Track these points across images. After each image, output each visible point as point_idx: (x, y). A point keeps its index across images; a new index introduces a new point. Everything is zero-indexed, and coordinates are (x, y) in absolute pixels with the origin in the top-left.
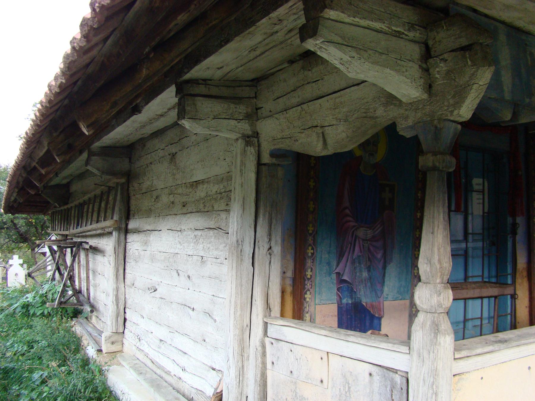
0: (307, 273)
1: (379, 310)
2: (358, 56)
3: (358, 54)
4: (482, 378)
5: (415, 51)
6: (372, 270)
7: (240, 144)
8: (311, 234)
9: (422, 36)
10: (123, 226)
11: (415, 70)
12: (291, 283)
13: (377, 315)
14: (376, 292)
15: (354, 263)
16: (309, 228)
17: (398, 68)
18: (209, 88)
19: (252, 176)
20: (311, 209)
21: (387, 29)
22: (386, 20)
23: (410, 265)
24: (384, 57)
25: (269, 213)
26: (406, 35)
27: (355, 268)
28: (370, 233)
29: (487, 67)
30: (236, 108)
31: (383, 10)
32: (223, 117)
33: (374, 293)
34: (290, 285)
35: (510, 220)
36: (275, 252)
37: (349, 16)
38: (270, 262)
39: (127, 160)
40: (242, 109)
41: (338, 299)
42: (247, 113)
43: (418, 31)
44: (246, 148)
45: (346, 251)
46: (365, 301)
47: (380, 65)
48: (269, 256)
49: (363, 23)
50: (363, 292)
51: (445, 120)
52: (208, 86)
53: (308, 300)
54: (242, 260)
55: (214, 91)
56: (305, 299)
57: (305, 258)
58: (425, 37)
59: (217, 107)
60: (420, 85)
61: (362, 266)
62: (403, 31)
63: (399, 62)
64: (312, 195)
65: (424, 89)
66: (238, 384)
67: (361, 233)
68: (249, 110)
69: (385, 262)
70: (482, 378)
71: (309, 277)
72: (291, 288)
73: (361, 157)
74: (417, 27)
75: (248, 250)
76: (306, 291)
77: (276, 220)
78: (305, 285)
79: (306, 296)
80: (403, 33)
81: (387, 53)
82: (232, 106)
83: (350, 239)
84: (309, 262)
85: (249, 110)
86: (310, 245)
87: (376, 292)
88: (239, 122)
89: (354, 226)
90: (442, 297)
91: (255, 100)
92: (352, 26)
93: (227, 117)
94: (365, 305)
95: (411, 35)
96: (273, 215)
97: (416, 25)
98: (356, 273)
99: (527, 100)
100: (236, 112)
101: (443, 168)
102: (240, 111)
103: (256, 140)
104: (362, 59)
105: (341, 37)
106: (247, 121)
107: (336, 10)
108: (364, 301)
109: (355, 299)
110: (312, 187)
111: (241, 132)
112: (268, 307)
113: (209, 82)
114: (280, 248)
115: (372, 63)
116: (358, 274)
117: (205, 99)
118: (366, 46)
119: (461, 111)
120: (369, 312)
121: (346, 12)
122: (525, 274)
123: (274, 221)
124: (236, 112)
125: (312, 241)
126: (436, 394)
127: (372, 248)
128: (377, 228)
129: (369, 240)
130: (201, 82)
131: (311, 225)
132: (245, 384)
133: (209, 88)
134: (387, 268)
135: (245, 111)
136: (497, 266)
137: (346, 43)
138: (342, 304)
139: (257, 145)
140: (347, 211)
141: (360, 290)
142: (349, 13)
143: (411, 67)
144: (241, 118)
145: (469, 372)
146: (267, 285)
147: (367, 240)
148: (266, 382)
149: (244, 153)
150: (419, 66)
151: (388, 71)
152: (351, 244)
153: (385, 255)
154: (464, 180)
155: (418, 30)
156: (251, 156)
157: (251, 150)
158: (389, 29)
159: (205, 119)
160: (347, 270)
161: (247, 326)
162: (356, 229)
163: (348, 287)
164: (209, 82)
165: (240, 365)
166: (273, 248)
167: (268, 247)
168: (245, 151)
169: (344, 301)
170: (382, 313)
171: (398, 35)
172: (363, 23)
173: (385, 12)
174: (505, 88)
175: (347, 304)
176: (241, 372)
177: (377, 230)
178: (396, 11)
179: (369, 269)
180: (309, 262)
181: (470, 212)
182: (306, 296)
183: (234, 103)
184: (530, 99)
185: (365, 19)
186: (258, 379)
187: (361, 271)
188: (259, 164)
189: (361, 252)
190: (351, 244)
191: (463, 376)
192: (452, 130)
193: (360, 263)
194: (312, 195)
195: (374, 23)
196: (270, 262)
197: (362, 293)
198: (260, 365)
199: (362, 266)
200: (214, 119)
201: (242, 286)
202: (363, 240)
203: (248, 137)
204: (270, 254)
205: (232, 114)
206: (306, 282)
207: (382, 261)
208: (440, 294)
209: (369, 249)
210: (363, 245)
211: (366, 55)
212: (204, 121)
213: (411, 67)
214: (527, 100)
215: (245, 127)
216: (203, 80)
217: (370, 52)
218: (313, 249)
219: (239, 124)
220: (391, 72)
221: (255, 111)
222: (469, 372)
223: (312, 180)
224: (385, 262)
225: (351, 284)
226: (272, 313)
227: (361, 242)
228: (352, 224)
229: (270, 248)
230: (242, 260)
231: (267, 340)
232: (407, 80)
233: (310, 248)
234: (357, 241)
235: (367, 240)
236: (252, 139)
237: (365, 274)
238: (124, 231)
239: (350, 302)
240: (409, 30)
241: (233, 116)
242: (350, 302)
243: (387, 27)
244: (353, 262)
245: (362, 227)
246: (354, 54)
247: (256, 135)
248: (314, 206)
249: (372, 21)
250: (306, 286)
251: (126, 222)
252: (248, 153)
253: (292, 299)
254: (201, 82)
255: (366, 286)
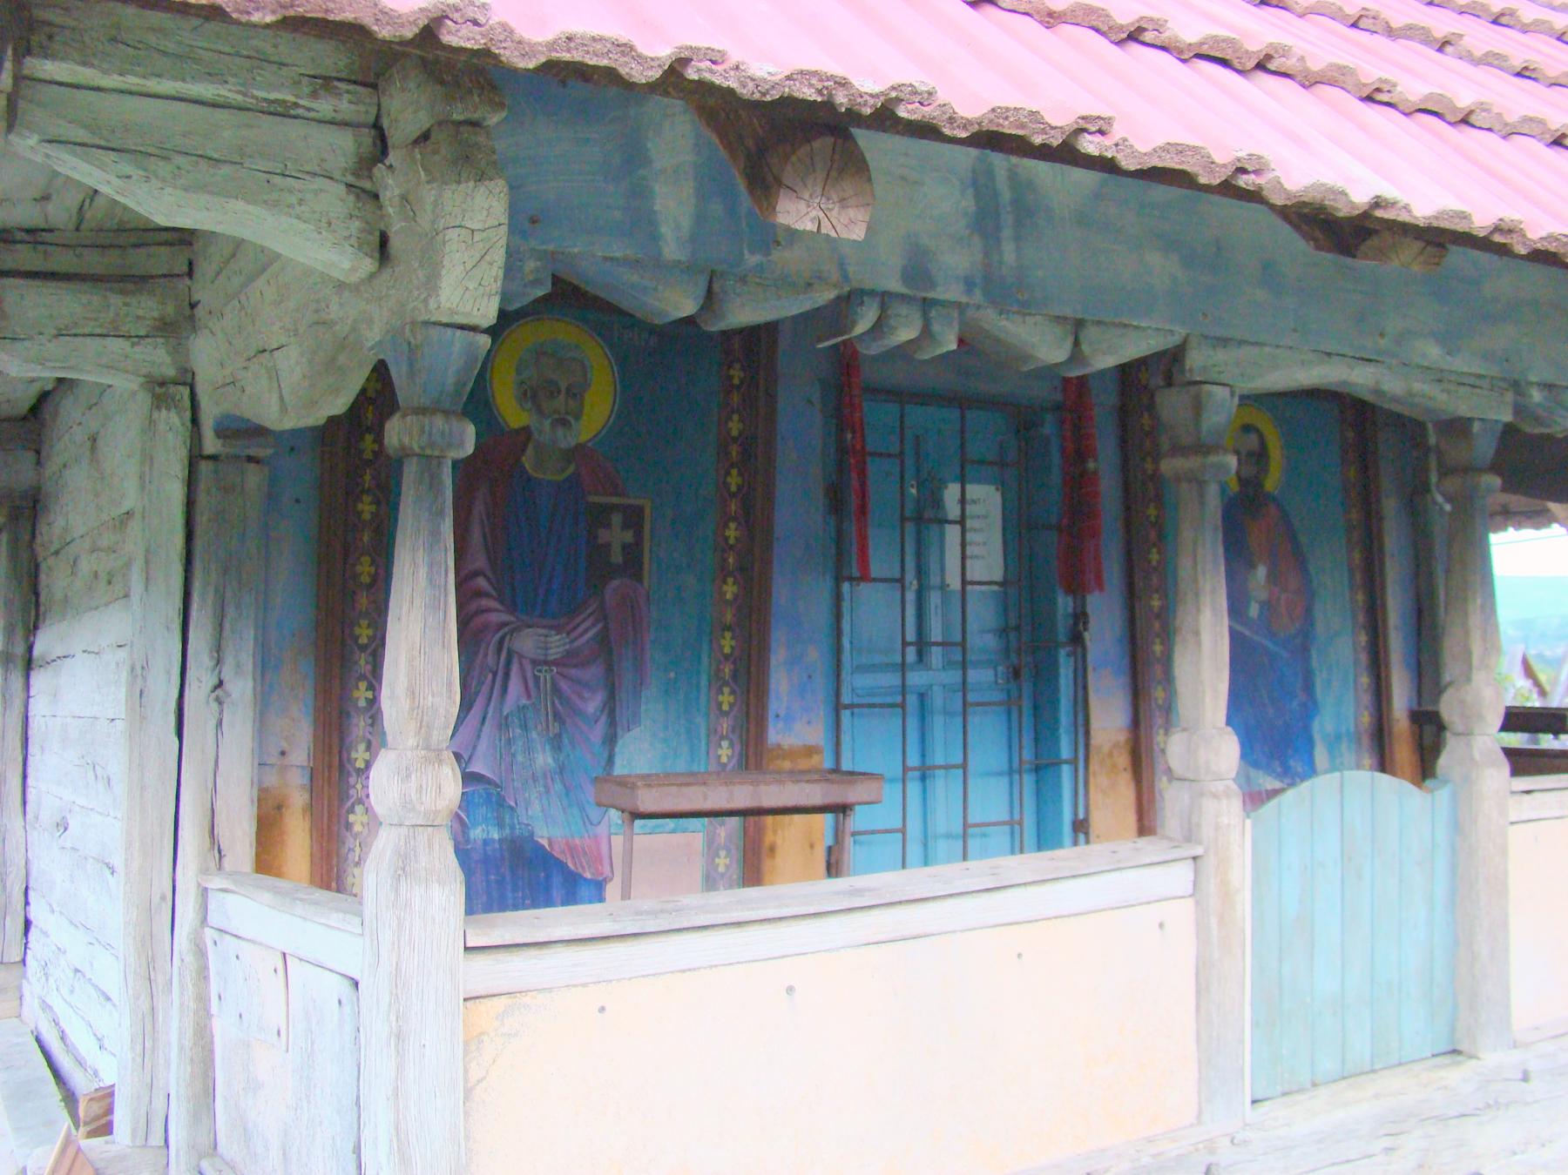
0: (354, 755)
1: (598, 859)
2: (142, 173)
3: (139, 168)
4: (602, 1009)
5: (343, 147)
6: (567, 749)
7: (144, 399)
8: (363, 648)
9: (362, 108)
10: (20, 649)
11: (333, 199)
12: (306, 780)
13: (588, 875)
14: (582, 810)
15: (507, 726)
16: (357, 631)
17: (275, 195)
18: (45, 252)
19: (175, 492)
20: (366, 579)
21: (240, 98)
22: (235, 75)
23: (703, 732)
24: (226, 170)
25: (217, 591)
26: (309, 109)
27: (509, 742)
28: (557, 644)
29: (471, 184)
30: (127, 304)
31: (228, 49)
32: (87, 331)
33: (576, 811)
34: (303, 787)
35: (1064, 604)
36: (235, 695)
37: (106, 72)
38: (220, 723)
39: (30, 457)
40: (147, 307)
41: (457, 826)
42: (162, 319)
43: (346, 97)
44: (156, 415)
45: (477, 694)
46: (546, 834)
47: (212, 193)
48: (215, 706)
49: (167, 86)
50: (538, 807)
51: (426, 323)
52: (40, 247)
53: (357, 828)
54: (143, 718)
55: (63, 261)
56: (349, 826)
57: (348, 714)
58: (374, 111)
59: (68, 303)
60: (346, 238)
61: (534, 735)
62: (292, 99)
63: (278, 180)
64: (366, 539)
65: (360, 248)
66: (140, 1060)
67: (527, 643)
68: (170, 310)
69: (612, 723)
70: (602, 1009)
71: (360, 764)
72: (307, 796)
73: (526, 431)
74: (343, 86)
75: (164, 690)
76: (353, 806)
77: (238, 607)
78: (349, 787)
79: (352, 818)
80: (296, 105)
81: (238, 159)
82: (116, 300)
83: (491, 660)
84: (362, 724)
85: (170, 310)
86: (363, 677)
87: (582, 810)
88: (133, 345)
89: (505, 624)
90: (413, 783)
91: (188, 282)
92: (128, 97)
93: (98, 331)
94: (545, 843)
95: (325, 107)
96: (229, 594)
97: (339, 80)
98: (514, 755)
99: (752, 260)
100: (127, 315)
101: (422, 448)
102: (140, 312)
103: (186, 391)
104: (154, 180)
105: (86, 127)
106: (160, 340)
107: (62, 59)
108: (543, 835)
109: (512, 828)
110: (367, 516)
111: (144, 371)
112: (215, 846)
113: (47, 237)
114: (250, 684)
115: (186, 190)
116: (520, 758)
117: (30, 282)
118: (168, 146)
119: (443, 298)
120: (562, 865)
121: (96, 62)
122: (1123, 760)
123: (231, 612)
124: (127, 315)
125: (369, 667)
126: (398, 1036)
127: (563, 685)
128: (581, 629)
129: (555, 663)
130: (20, 236)
131: (364, 623)
132: (161, 1061)
133: (45, 252)
134: (620, 743)
135: (156, 314)
136: (1036, 740)
137: (103, 143)
138: (468, 841)
139: (187, 403)
140: (481, 582)
141: (528, 803)
142: (105, 66)
143: (316, 193)
144: (142, 333)
145: (550, 990)
146: (210, 785)
147: (546, 663)
148: (212, 1051)
149: (150, 425)
150: (349, 186)
151: (240, 205)
152: (495, 674)
153: (610, 707)
154: (914, 491)
155: (348, 92)
156: (170, 436)
157: (173, 422)
158: (245, 95)
159: (31, 338)
160: (483, 746)
161: (163, 898)
162: (512, 632)
163: (489, 795)
164: (47, 237)
165: (146, 1006)
166: (228, 686)
167: (215, 681)
168: (152, 423)
169: (477, 833)
170: (607, 869)
171: (282, 111)
172: (167, 86)
173: (238, 54)
174: (665, 230)
175: (486, 842)
176: (149, 1027)
177: (581, 635)
178: (276, 46)
179: (557, 744)
180: (362, 724)
181: (934, 580)
182: (352, 818)
183: (123, 292)
184: (767, 254)
185: (159, 76)
186: (187, 1044)
187: (529, 750)
188: (195, 458)
189: (529, 696)
190: (495, 674)
191: (527, 999)
192: (457, 348)
193: (525, 727)
194: (366, 539)
195: (189, 86)
196: (220, 723)
197: (536, 809)
198: (192, 1005)
199: (534, 735)
200: (57, 336)
201: (143, 788)
202: (535, 663)
203: (162, 384)
204: (219, 701)
205: (114, 321)
206: (352, 780)
207: (604, 719)
208: (408, 776)
209: (556, 690)
210: (537, 679)
211: (164, 169)
212: (27, 344)
213: (316, 193)
214: (752, 260)
215: (159, 358)
216: (30, 231)
217: (181, 160)
218: (371, 687)
219: (137, 349)
220: (251, 208)
221: (187, 312)
222: (550, 990)
223: (367, 499)
224: (612, 723)
225: (497, 786)
226: (226, 861)
227: (528, 667)
228: (495, 618)
229: (220, 684)
230: (143, 718)
231: (209, 934)
232: (304, 226)
233: (363, 685)
234: (515, 668)
235: (546, 663)
236: (172, 389)
237: (544, 759)
238: (20, 664)
239: (496, 836)
240: (314, 95)
241: (116, 329)
242: (496, 836)
243: (239, 92)
244: (503, 724)
245: (530, 627)
246: (127, 169)
247: (187, 379)
248: (373, 570)
249: (184, 80)
250: (352, 792)
251: (27, 638)
252: (162, 427)
253: (307, 825)
254: (20, 236)
255: (548, 791)
